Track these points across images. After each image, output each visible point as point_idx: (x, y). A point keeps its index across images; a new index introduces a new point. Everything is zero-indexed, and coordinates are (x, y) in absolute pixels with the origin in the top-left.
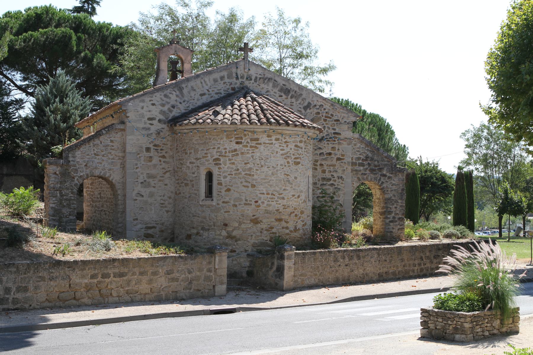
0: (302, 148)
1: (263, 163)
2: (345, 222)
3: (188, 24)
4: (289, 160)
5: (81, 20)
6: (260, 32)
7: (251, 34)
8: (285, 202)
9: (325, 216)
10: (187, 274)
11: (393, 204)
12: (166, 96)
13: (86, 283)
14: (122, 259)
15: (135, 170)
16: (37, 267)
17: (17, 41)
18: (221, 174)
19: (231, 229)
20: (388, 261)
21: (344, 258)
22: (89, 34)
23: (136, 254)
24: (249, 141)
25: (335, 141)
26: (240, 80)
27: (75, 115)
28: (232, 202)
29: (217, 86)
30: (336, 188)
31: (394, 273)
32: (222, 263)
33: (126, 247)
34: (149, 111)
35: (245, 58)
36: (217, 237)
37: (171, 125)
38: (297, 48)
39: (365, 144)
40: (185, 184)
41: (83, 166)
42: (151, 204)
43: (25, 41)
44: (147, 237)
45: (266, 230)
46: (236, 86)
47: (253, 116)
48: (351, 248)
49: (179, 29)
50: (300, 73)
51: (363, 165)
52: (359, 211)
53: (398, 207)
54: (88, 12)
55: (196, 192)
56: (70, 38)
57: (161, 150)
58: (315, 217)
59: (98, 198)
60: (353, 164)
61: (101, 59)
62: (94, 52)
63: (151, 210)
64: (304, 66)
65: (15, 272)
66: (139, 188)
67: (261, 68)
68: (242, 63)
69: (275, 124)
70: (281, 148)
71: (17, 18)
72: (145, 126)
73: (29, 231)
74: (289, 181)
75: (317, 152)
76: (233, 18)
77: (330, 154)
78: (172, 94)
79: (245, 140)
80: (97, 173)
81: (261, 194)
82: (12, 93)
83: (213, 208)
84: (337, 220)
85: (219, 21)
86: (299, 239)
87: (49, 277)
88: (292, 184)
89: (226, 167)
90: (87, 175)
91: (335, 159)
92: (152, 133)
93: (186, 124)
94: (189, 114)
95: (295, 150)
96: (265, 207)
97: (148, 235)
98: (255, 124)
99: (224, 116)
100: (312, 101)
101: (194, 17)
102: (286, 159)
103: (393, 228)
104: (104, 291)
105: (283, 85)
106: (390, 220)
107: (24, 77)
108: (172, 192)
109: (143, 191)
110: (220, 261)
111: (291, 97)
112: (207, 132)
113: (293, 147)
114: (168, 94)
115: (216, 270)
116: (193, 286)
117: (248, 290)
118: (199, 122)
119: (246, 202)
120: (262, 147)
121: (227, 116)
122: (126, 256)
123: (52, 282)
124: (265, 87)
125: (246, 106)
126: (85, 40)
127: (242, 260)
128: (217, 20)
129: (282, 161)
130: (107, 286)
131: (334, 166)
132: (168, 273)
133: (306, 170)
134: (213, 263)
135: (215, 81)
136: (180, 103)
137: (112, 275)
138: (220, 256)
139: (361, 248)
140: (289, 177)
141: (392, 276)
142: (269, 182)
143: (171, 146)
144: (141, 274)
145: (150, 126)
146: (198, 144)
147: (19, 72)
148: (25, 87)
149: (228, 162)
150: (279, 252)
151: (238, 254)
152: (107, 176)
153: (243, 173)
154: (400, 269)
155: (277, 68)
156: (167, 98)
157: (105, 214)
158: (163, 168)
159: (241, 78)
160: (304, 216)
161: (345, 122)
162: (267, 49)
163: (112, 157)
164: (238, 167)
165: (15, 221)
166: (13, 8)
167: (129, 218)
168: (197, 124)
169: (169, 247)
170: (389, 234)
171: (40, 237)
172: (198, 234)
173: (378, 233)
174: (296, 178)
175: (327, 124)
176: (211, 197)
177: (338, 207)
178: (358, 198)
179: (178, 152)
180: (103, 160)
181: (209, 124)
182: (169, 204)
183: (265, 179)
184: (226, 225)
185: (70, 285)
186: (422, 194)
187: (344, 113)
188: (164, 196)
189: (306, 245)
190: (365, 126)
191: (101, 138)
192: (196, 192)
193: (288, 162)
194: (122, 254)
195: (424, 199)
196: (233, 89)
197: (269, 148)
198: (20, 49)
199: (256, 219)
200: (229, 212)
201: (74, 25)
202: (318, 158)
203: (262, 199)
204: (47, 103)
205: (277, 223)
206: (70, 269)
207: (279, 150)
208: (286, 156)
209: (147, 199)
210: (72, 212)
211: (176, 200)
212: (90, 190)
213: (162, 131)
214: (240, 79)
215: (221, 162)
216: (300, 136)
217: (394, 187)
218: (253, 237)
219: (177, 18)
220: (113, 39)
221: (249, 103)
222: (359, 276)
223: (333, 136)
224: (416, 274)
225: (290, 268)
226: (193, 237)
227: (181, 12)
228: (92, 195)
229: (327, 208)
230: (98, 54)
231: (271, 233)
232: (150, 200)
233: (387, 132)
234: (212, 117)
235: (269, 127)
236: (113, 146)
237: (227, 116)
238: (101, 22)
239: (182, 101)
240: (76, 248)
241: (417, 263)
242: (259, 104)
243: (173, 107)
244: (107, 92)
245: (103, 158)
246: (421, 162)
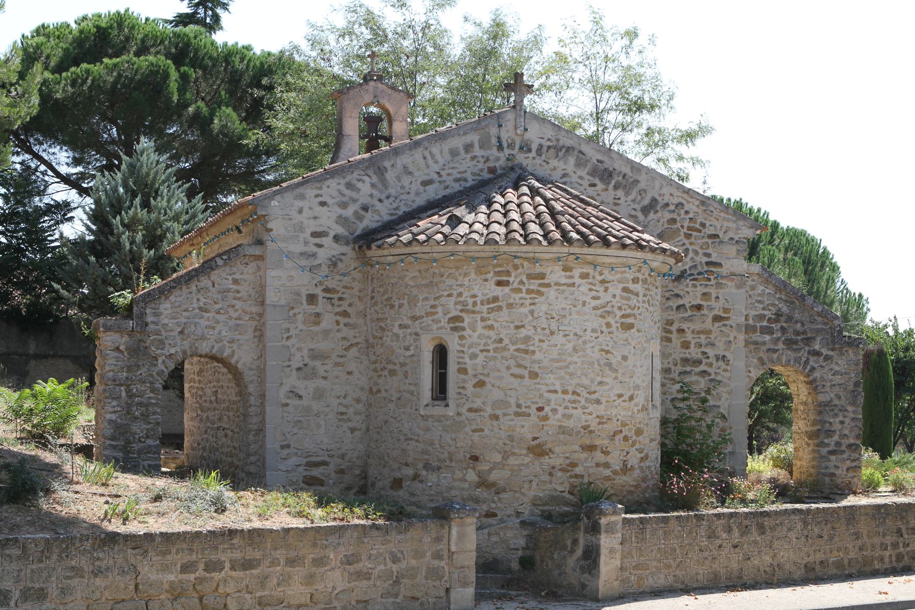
0: (637, 295)
1: (554, 326)
2: (732, 453)
3: (406, 43)
4: (610, 319)
5: (189, 40)
6: (554, 55)
7: (537, 63)
8: (601, 410)
9: (688, 441)
10: (390, 564)
11: (836, 415)
12: (349, 186)
13: (172, 582)
14: (249, 531)
15: (284, 342)
16: (67, 548)
17: (59, 83)
18: (465, 349)
19: (487, 468)
20: (826, 537)
21: (729, 530)
22: (204, 68)
23: (281, 520)
24: (525, 280)
25: (709, 280)
26: (507, 151)
27: (173, 233)
28: (489, 410)
29: (457, 165)
30: (712, 380)
31: (839, 565)
32: (465, 539)
33: (260, 503)
34: (315, 218)
35: (517, 106)
36: (456, 484)
37: (360, 247)
38: (630, 90)
39: (775, 286)
41: (176, 333)
42: (317, 415)
43: (74, 83)
44: (310, 483)
45: (560, 470)
46: (497, 165)
47: (533, 227)
48: (746, 510)
49: (387, 54)
50: (638, 142)
51: (768, 331)
52: (765, 433)
53: (847, 421)
54: (205, 25)
55: (412, 388)
56: (166, 75)
57: (340, 299)
58: (667, 442)
59: (211, 402)
60: (749, 329)
61: (228, 118)
62: (215, 104)
63: (319, 426)
64: (645, 127)
65: (19, 558)
66: (292, 380)
67: (549, 126)
68: (510, 116)
69: (579, 244)
70: (594, 293)
71: (58, 37)
73: (54, 470)
74: (609, 365)
75: (670, 303)
76: (498, 31)
77: (699, 307)
78: (363, 182)
79: (516, 277)
80: (204, 348)
81: (550, 391)
82: (50, 189)
83: (448, 422)
84: (715, 449)
85: (470, 37)
86: (632, 489)
87: (91, 568)
88: (616, 371)
89: (476, 334)
90: (184, 352)
91: (710, 319)
92: (320, 265)
93: (392, 245)
94: (398, 224)
95: (622, 297)
96: (560, 421)
97: (316, 483)
98: (536, 242)
99: (471, 226)
100: (660, 195)
101: (418, 29)
102: (604, 317)
103: (837, 467)
104: (209, 600)
105: (598, 161)
106: (830, 449)
107: (74, 158)
108: (362, 389)
109: (302, 386)
110: (462, 536)
111: (616, 188)
112: (435, 260)
113: (618, 292)
114: (354, 182)
115: (451, 554)
116: (402, 589)
117: (523, 598)
118: (417, 240)
119: (519, 410)
120: (552, 293)
121: (477, 226)
122: (257, 524)
123: (97, 579)
124: (558, 166)
125: (519, 206)
126: (196, 80)
127: (510, 534)
128: (465, 36)
129: (596, 322)
130: (217, 589)
131: (708, 332)
132: (349, 561)
133: (648, 341)
134: (445, 541)
135: (454, 153)
136: (380, 201)
137: (227, 565)
138: (462, 525)
139: (767, 508)
140: (609, 356)
141: (835, 571)
142: (567, 367)
143: (360, 291)
144: (291, 562)
145: (315, 249)
146: (417, 286)
147: (65, 148)
148: (78, 179)
149: (480, 325)
150: (588, 518)
151: (502, 521)
152: (225, 355)
153: (512, 348)
154: (852, 555)
155: (590, 133)
156: (353, 190)
157: (226, 436)
158: (344, 339)
159: (508, 147)
160: (644, 440)
161: (732, 239)
162: (569, 94)
163: (235, 315)
164: (502, 336)
165: (29, 450)
166: (52, 19)
167: (272, 443)
168: (415, 243)
169: (350, 505)
170: (827, 479)
171: (77, 483)
172: (416, 477)
173: (804, 477)
174: (625, 358)
175: (691, 244)
176: (445, 399)
177: (717, 420)
178: (763, 403)
179: (376, 304)
180: (218, 322)
181: (438, 243)
182: (355, 413)
183: (558, 361)
184: (475, 458)
185: (137, 586)
186: (898, 397)
187: (728, 220)
188: (345, 397)
189: (648, 502)
190: (776, 254)
191: (214, 275)
192: (412, 388)
193: (608, 325)
194: (250, 521)
195: (902, 408)
196: (492, 170)
197: (567, 293)
198: (64, 99)
199: (540, 446)
200: (482, 430)
201: (173, 50)
202: (674, 315)
203: (553, 403)
204: (117, 207)
205: (585, 455)
206: (137, 551)
208: (604, 311)
209: (308, 406)
210: (153, 430)
211: (370, 405)
212: (197, 385)
213: (341, 260)
214: (506, 150)
215: (465, 324)
216: (633, 269)
217: (838, 379)
218: (534, 484)
219: (384, 31)
220: (254, 77)
221: (525, 198)
222: (762, 569)
223: (706, 268)
224: (887, 565)
225: (612, 551)
226: (405, 484)
227: (391, 19)
228: (201, 396)
229: (693, 423)
230: (223, 108)
231: (571, 477)
232: (316, 406)
233: (822, 266)
234: (446, 229)
235: (566, 250)
236: (238, 292)
237: (477, 226)
238: (230, 44)
239: (383, 197)
240: (151, 507)
241: (889, 543)
242: (547, 201)
243: (365, 208)
244: (243, 187)
245: (218, 317)
246: (896, 330)
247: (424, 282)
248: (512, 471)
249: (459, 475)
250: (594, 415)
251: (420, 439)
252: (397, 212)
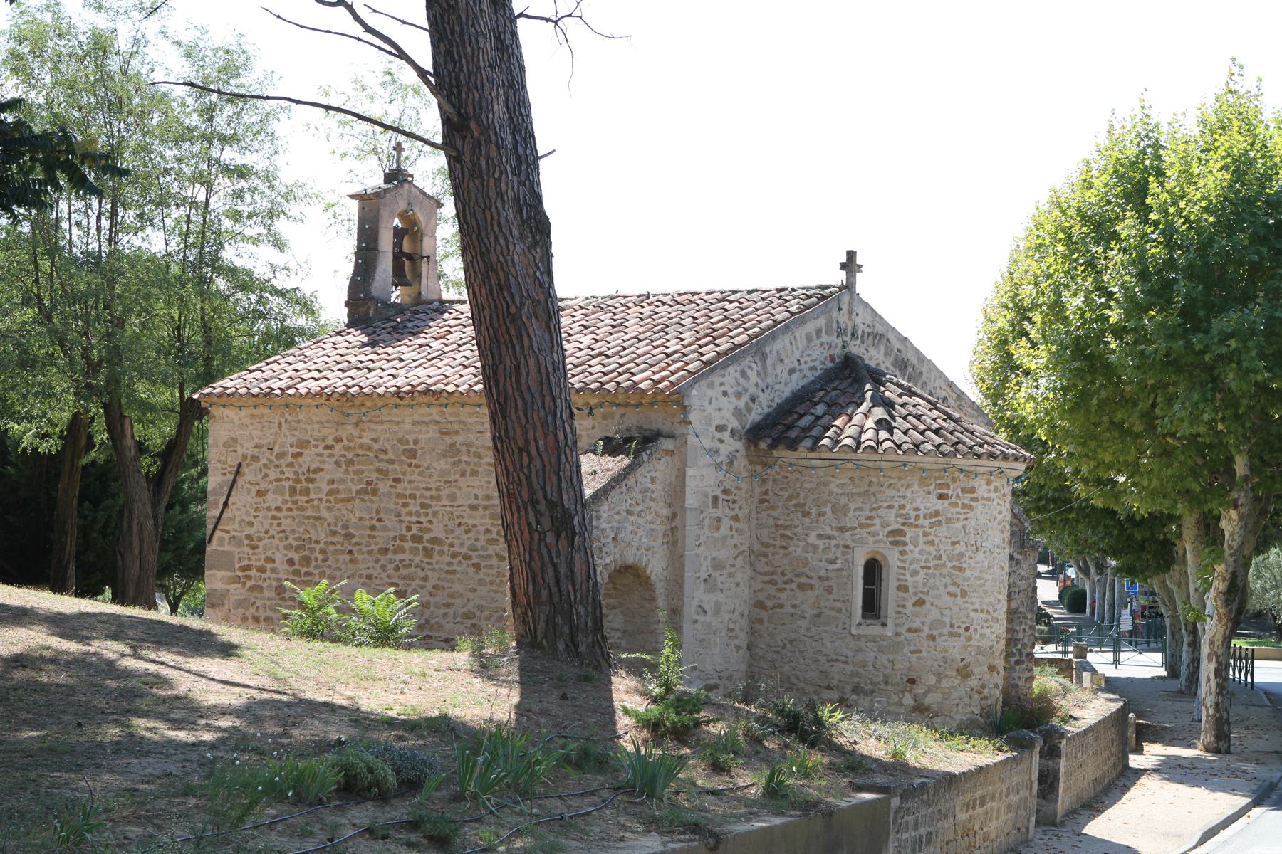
18: (906, 566)
36: (892, 708)
89: (917, 550)
145: (717, 444)
149: (922, 539)
153: (949, 565)
184: (912, 681)
200: (920, 652)
215: (907, 539)
248: (943, 693)
249: (895, 699)
251: (849, 660)
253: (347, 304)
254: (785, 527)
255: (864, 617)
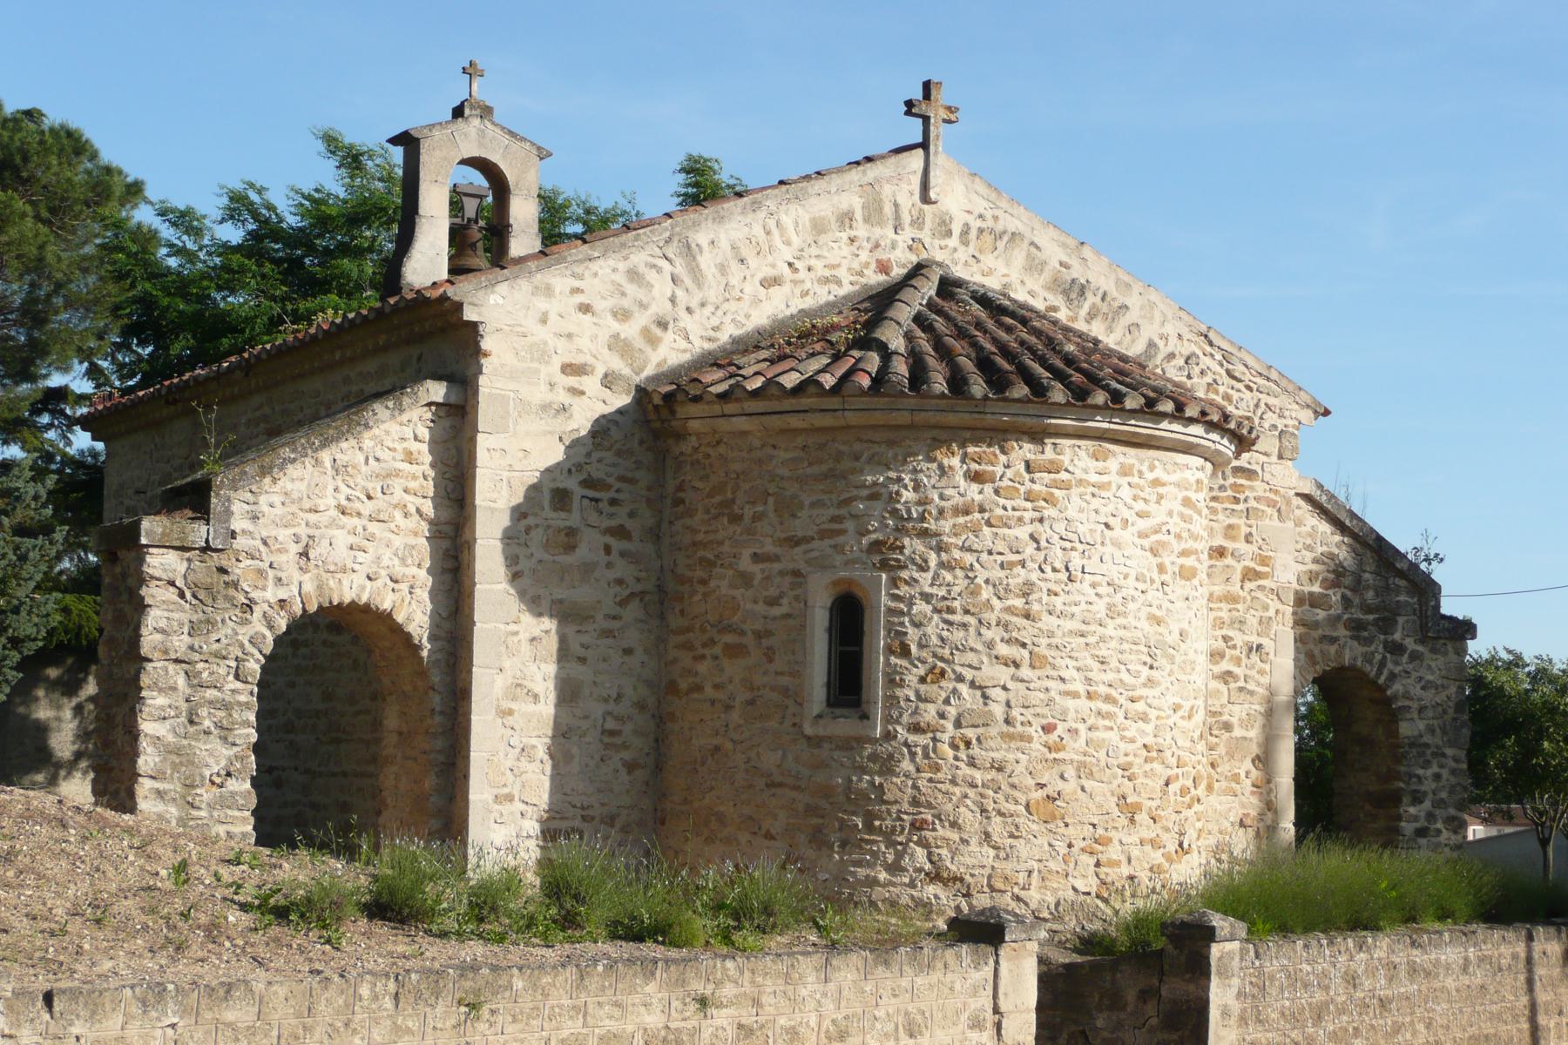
12: (634, 275)
34: (570, 336)
40: (727, 647)
53: (1445, 773)
55: (785, 681)
57: (613, 502)
72: (549, 397)
78: (659, 270)
91: (1237, 577)
113: (1177, 506)
114: (642, 269)
135: (819, 227)
158: (620, 582)
159: (913, 223)
193: (1161, 569)
207: (1132, 517)
217: (1429, 697)
247: (815, 469)
250: (1139, 744)
252: (718, 335)
253: (509, 225)
254: (704, 545)
255: (830, 704)
